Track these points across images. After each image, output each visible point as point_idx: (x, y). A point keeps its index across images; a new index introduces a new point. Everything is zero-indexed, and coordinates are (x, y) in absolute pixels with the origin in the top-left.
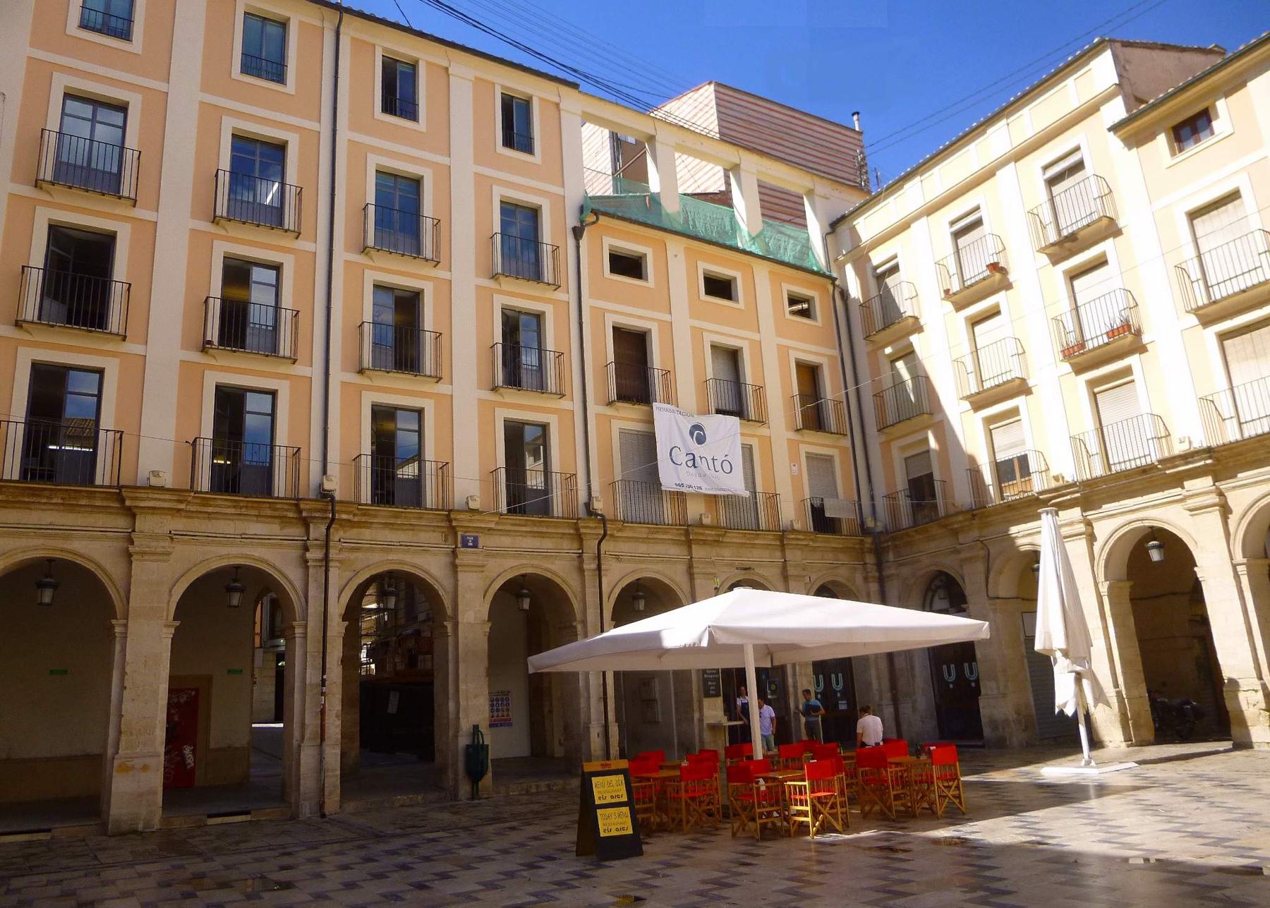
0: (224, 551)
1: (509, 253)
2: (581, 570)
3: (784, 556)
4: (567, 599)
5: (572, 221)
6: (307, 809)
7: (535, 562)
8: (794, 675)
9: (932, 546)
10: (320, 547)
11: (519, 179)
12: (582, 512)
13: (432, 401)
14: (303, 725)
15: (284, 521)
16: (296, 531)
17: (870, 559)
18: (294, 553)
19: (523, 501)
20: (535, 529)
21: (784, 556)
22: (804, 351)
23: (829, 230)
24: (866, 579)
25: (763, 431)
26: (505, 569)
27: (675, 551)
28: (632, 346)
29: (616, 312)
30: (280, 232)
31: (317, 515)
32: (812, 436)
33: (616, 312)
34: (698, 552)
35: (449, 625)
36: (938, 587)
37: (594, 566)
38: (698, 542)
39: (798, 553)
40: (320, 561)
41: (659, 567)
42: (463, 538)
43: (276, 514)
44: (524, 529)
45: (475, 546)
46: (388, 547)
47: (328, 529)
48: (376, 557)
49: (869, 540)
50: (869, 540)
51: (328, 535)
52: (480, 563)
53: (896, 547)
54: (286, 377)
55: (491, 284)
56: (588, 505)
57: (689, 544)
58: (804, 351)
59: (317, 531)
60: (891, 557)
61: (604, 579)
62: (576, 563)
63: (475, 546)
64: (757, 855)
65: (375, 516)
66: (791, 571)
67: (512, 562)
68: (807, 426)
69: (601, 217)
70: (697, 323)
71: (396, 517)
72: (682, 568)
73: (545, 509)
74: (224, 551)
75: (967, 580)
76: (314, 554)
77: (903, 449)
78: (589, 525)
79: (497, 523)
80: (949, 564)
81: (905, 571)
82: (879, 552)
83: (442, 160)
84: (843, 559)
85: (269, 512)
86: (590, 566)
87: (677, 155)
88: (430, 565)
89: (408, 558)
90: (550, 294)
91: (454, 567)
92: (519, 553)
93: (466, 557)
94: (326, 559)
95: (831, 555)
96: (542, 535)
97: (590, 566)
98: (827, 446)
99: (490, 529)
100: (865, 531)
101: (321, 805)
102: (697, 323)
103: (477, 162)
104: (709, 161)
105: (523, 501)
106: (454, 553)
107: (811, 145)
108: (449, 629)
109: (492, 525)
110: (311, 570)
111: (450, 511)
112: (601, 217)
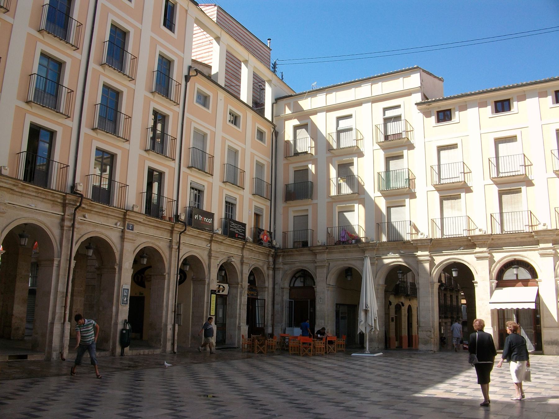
0: (26, 215)
1: (50, 18)
2: (62, 227)
3: (242, 253)
4: (114, 253)
5: (185, 72)
6: (55, 355)
7: (153, 241)
8: (240, 309)
9: (302, 258)
10: (70, 220)
11: (166, 44)
12: (68, 191)
13: (61, 128)
14: (54, 313)
15: (54, 202)
16: (58, 211)
17: (271, 259)
18: (57, 221)
19: (153, 209)
20: (156, 225)
21: (242, 253)
22: (260, 157)
23: (274, 101)
24: (268, 268)
25: (126, 145)
26: (142, 242)
27: (204, 244)
28: (112, 98)
29: (198, 123)
30: (121, 75)
31: (72, 203)
32: (257, 198)
33: (198, 123)
34: (214, 246)
35: (117, 268)
36: (300, 276)
37: (177, 247)
38: (217, 242)
39: (248, 252)
40: (70, 227)
41: (198, 251)
42: (128, 224)
43: (53, 199)
44: (152, 224)
45: (132, 230)
46: (96, 225)
47: (75, 210)
48: (90, 229)
49: (273, 251)
50: (273, 251)
51: (75, 214)
52: (134, 239)
53: (283, 255)
54: (208, 181)
55: (150, 96)
56: (73, 187)
57: (211, 241)
58: (260, 157)
59: (70, 211)
60: (280, 260)
61: (75, 233)
62: (168, 244)
63: (132, 230)
64: (91, 411)
65: (95, 207)
66: (245, 261)
67: (145, 240)
68: (153, 148)
69: (199, 74)
70: (254, 152)
71: (104, 210)
72: (206, 253)
73: (45, 182)
74: (26, 215)
75: (317, 275)
76: (67, 223)
77: (294, 211)
78: (72, 200)
79: (144, 220)
80: (309, 267)
81: (286, 267)
82: (275, 257)
83: (139, 25)
84: (262, 258)
85: (50, 198)
86: (175, 247)
87: (195, 25)
88: (112, 237)
89: (103, 231)
90: (70, 52)
91: (122, 238)
92: (148, 236)
93: (128, 234)
94: (73, 225)
95: (257, 255)
96: (157, 228)
97: (175, 247)
98: (262, 204)
99: (140, 222)
100: (273, 247)
101: (61, 354)
102: (254, 152)
103: (152, 31)
104: (208, 33)
105: (153, 209)
106: (123, 231)
107: (254, 42)
108: (117, 270)
109: (141, 220)
110: (65, 232)
111: (127, 210)
112: (199, 74)
